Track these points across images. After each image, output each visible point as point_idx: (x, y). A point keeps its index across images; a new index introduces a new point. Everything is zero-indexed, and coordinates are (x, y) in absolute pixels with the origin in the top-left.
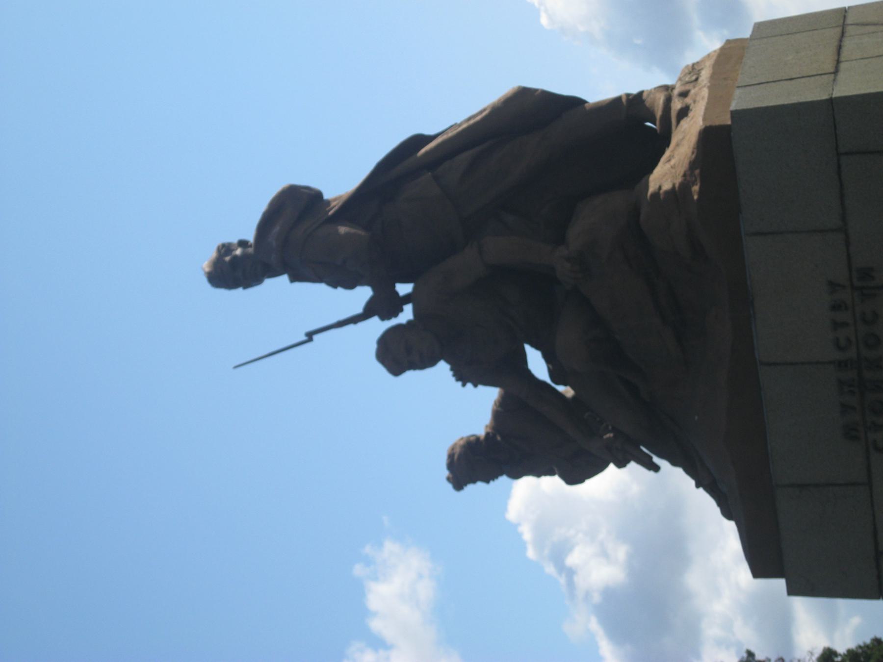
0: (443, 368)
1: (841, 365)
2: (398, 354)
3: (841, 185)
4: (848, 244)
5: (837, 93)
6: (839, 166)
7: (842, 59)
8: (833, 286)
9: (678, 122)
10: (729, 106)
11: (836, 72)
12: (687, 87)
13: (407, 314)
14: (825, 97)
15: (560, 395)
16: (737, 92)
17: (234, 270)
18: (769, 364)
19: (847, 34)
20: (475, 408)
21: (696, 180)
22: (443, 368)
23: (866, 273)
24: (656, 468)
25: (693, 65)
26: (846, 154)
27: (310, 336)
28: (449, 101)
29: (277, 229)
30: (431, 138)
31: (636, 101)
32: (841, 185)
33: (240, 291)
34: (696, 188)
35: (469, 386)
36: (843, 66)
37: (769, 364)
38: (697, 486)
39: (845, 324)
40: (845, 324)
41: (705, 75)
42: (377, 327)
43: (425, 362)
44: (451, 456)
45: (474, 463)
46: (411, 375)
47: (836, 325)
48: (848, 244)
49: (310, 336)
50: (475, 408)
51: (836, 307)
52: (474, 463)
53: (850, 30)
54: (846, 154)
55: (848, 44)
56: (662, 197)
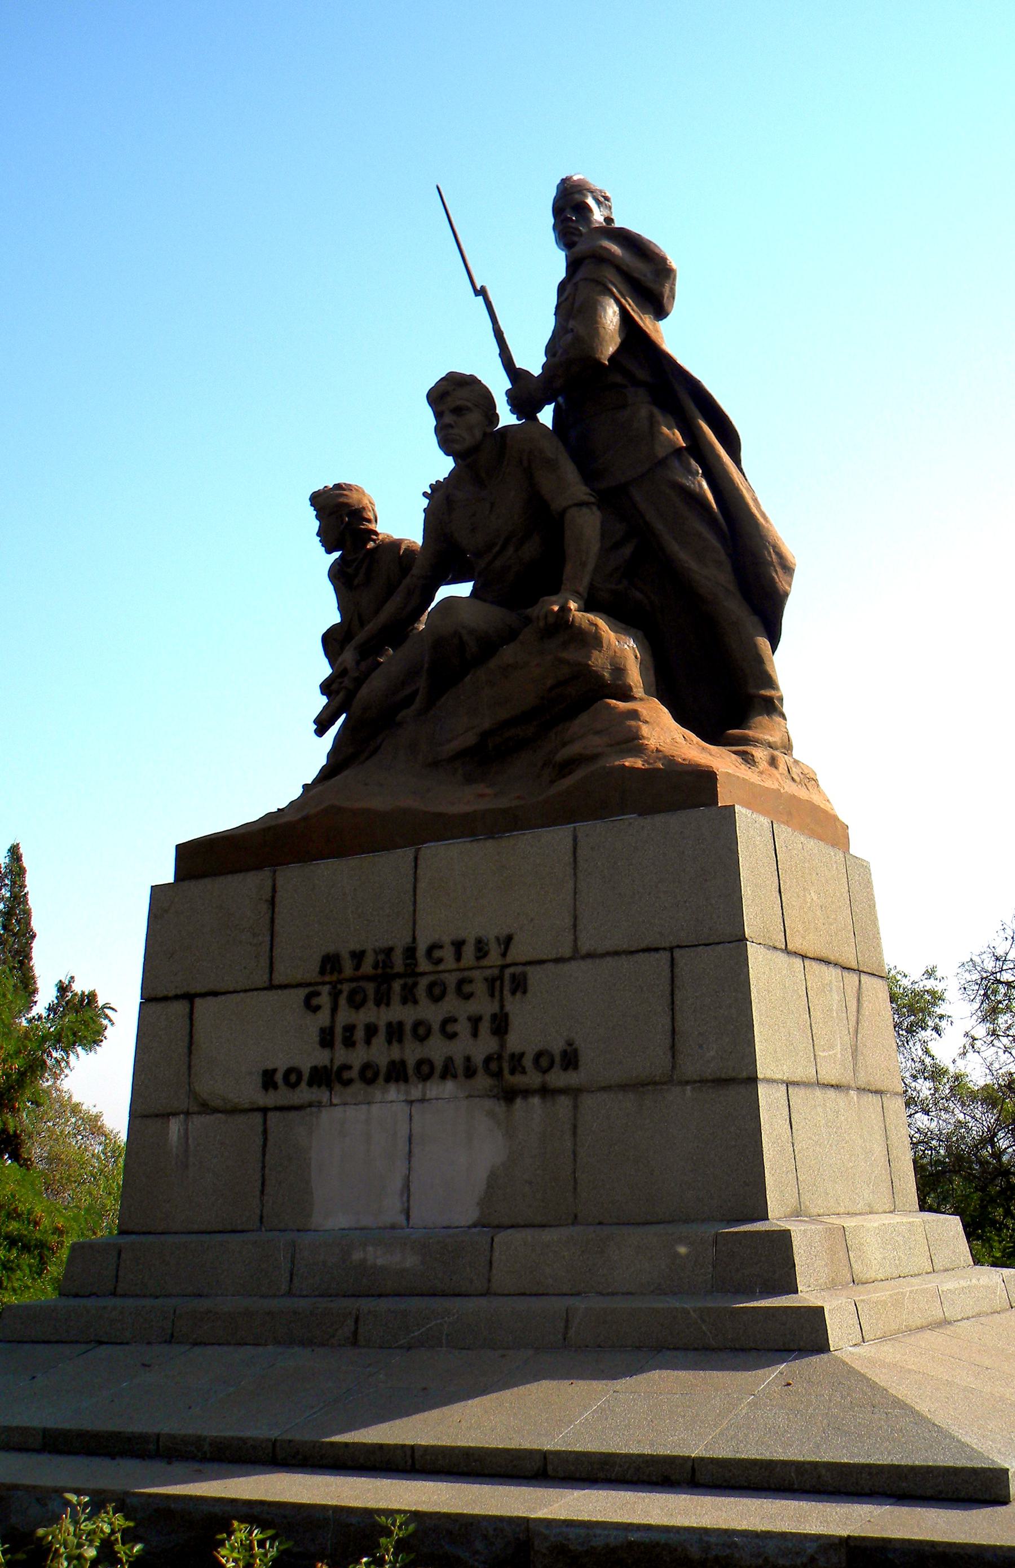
0: (443, 466)
1: (410, 952)
2: (455, 400)
3: (632, 953)
4: (558, 960)
5: (754, 953)
6: (657, 950)
7: (807, 962)
8: (508, 941)
9: (735, 753)
10: (747, 805)
11: (786, 951)
12: (782, 767)
13: (506, 417)
14: (748, 932)
15: (417, 618)
16: (765, 821)
17: (570, 205)
18: (416, 859)
19: (846, 973)
20: (401, 519)
21: (649, 764)
22: (443, 466)
23: (520, 985)
24: (321, 730)
25: (816, 781)
26: (672, 959)
27: (481, 292)
28: (777, 481)
29: (616, 249)
30: (737, 462)
31: (771, 707)
32: (632, 953)
33: (551, 220)
34: (639, 763)
35: (425, 502)
36: (798, 962)
37: (416, 859)
38: (305, 786)
39: (458, 957)
40: (458, 957)
41: (802, 793)
42: (498, 385)
43: (446, 441)
44: (349, 487)
45: (340, 517)
46: (428, 419)
47: (459, 945)
48: (558, 960)
49: (481, 292)
50: (401, 519)
51: (481, 949)
52: (340, 517)
53: (852, 978)
54: (672, 959)
55: (832, 974)
56: (633, 723)
